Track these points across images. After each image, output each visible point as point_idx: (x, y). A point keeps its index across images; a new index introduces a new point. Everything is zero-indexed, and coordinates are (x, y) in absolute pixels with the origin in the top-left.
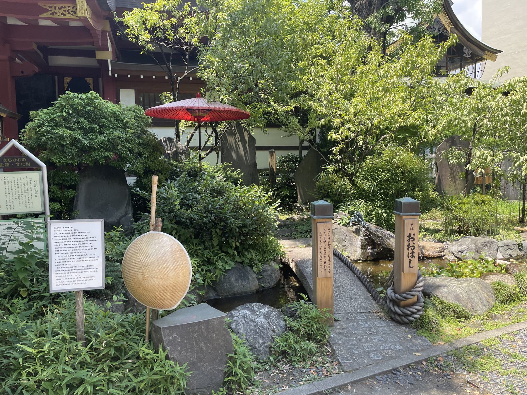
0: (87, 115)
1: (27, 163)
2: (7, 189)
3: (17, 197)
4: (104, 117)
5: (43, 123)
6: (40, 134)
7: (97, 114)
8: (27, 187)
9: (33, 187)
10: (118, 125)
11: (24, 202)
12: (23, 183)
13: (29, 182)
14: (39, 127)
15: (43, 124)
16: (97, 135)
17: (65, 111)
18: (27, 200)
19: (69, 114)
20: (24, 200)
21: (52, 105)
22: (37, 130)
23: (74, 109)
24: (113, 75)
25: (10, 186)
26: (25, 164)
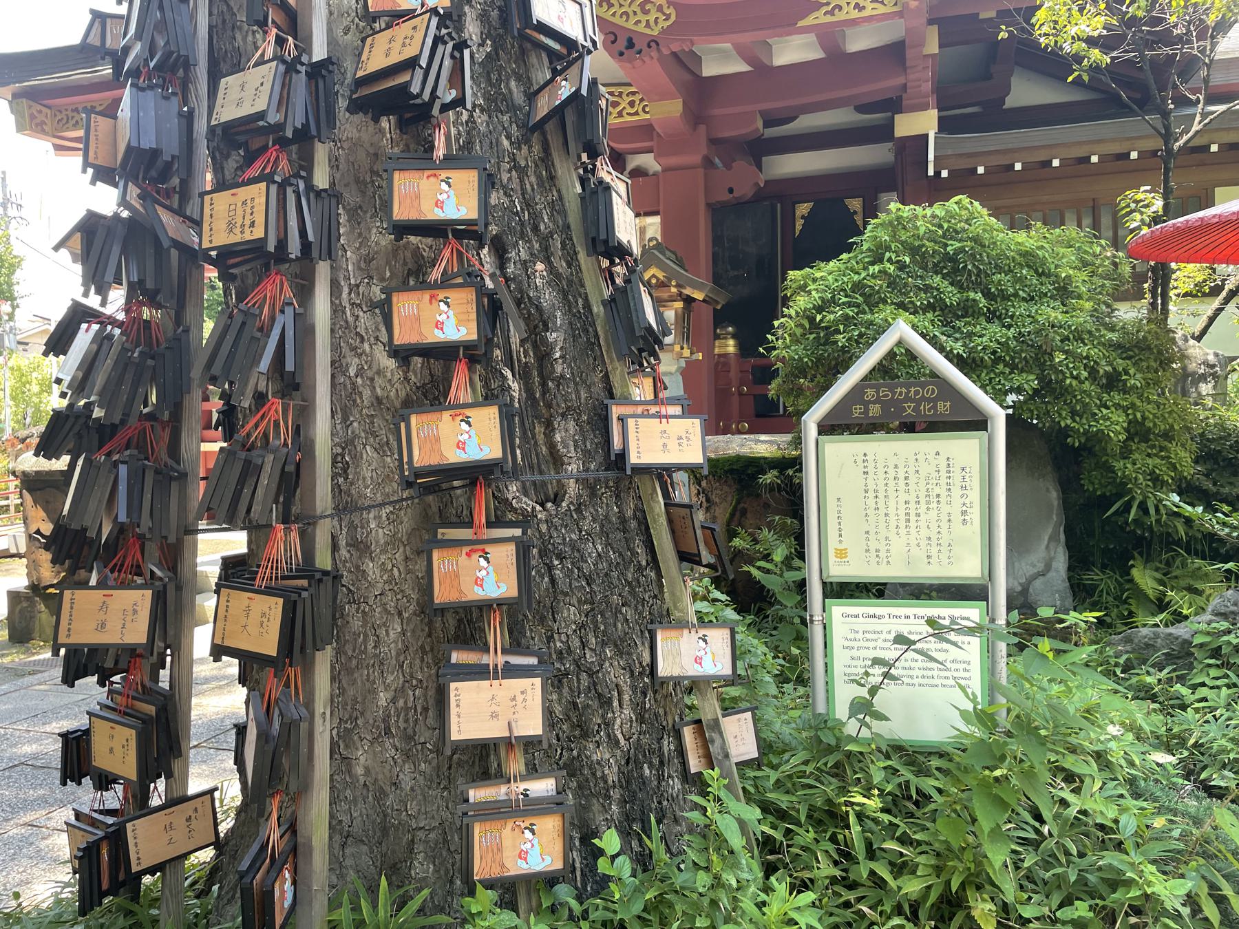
0: (951, 266)
1: (940, 404)
2: (871, 494)
3: (902, 524)
4: (999, 269)
5: (833, 297)
6: (827, 328)
7: (981, 261)
8: (937, 490)
9: (957, 492)
10: (1044, 289)
11: (923, 543)
12: (923, 474)
13: (943, 468)
14: (820, 309)
15: (833, 301)
16: (982, 320)
17: (890, 260)
18: (934, 538)
19: (902, 267)
20: (924, 533)
21: (849, 249)
22: (819, 317)
23: (914, 251)
24: (937, 173)
25: (881, 483)
26: (935, 407)
